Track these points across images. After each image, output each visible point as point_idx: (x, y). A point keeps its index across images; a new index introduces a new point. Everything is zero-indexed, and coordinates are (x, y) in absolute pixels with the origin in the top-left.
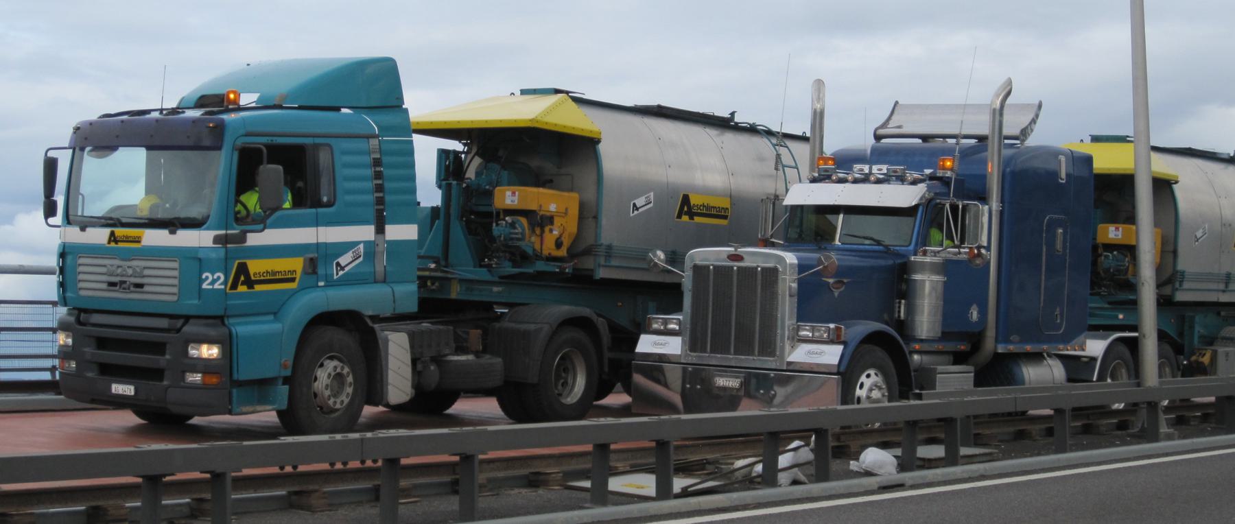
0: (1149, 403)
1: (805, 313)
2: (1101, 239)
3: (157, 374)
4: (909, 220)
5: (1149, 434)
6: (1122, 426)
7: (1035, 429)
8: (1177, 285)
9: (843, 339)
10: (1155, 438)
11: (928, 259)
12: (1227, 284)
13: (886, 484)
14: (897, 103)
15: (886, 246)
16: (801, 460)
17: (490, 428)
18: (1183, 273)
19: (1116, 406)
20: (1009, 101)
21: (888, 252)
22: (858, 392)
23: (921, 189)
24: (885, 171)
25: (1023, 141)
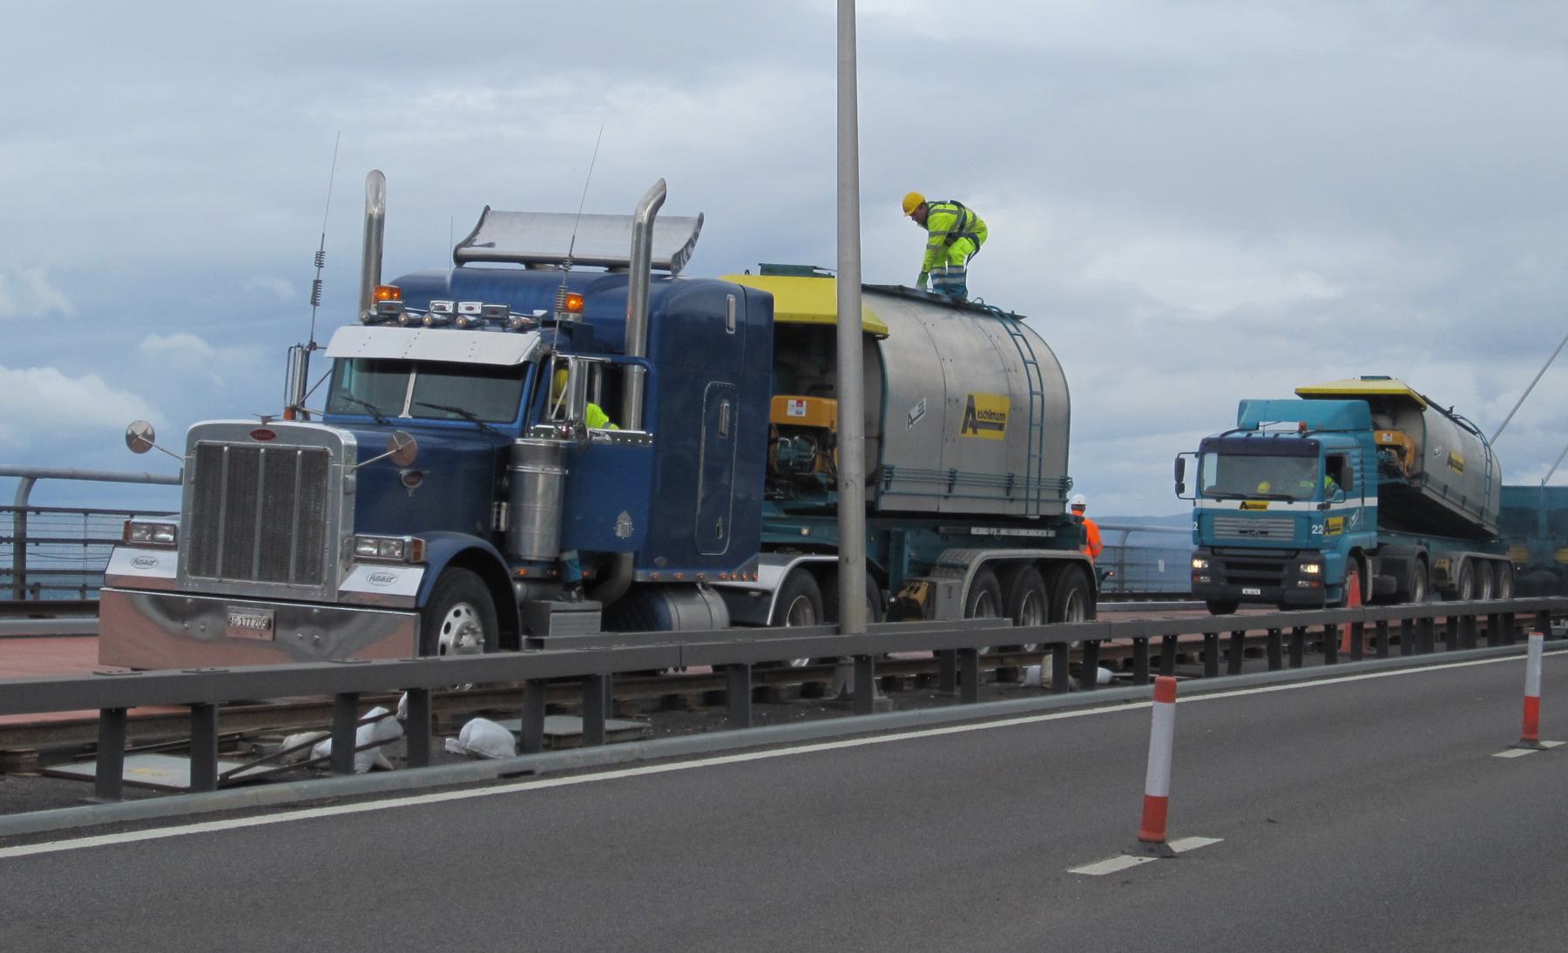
0: (858, 658)
1: (368, 518)
2: (775, 417)
3: (1277, 582)
4: (513, 384)
5: (855, 703)
6: (811, 691)
7: (692, 693)
8: (882, 487)
9: (423, 558)
10: (865, 707)
11: (542, 442)
12: (950, 486)
13: (507, 771)
14: (487, 209)
15: (479, 422)
16: (385, 737)
17: (145, 674)
18: (891, 470)
19: (796, 663)
20: (661, 212)
21: (482, 431)
22: (443, 637)
23: (532, 339)
24: (479, 311)
25: (676, 271)
